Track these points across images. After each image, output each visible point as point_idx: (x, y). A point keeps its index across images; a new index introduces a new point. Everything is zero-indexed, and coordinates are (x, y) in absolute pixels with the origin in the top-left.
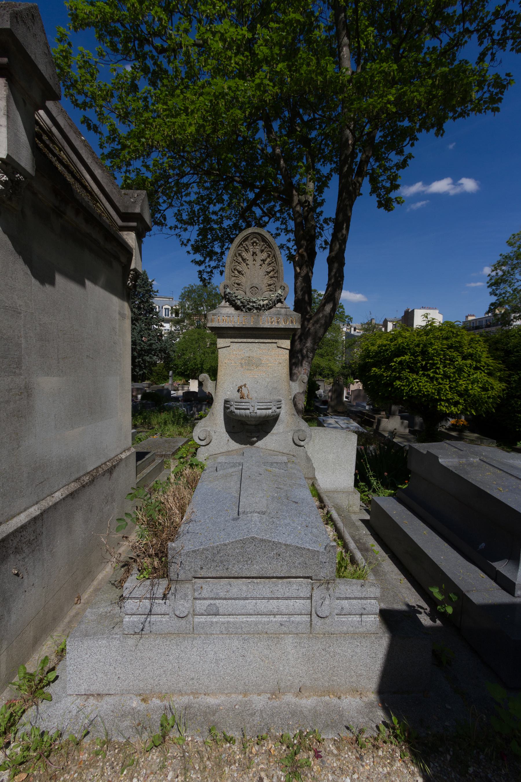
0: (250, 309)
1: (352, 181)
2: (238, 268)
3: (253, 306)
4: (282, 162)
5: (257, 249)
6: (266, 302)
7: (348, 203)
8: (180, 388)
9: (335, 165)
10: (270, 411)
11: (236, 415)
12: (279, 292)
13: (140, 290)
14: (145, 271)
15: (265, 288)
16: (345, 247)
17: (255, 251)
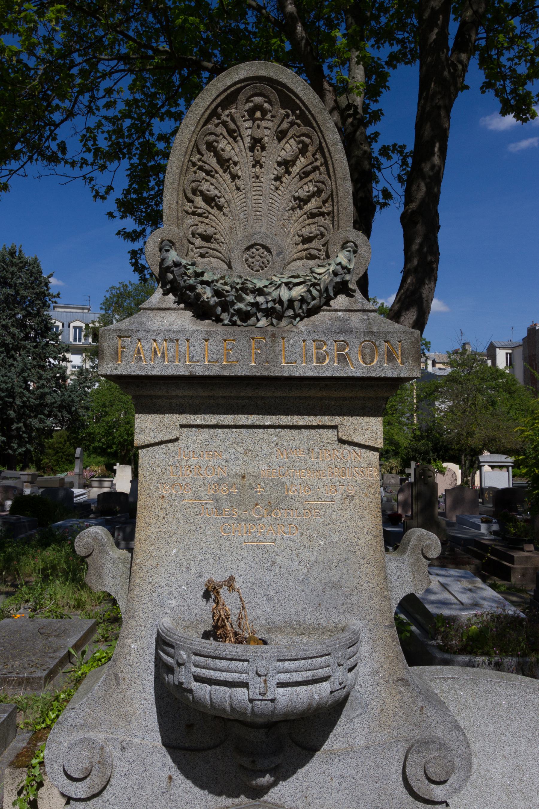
0: (245, 316)
1: (447, 59)
2: (205, 187)
3: (256, 305)
4: (299, 29)
5: (266, 130)
6: (298, 291)
7: (441, 103)
8: (95, 484)
9: (399, 47)
10: (326, 686)
11: (197, 702)
12: (342, 258)
13: (25, 294)
14: (36, 259)
15: (292, 251)
16: (439, 192)
17: (258, 134)
